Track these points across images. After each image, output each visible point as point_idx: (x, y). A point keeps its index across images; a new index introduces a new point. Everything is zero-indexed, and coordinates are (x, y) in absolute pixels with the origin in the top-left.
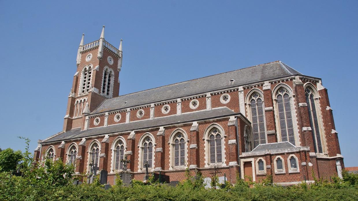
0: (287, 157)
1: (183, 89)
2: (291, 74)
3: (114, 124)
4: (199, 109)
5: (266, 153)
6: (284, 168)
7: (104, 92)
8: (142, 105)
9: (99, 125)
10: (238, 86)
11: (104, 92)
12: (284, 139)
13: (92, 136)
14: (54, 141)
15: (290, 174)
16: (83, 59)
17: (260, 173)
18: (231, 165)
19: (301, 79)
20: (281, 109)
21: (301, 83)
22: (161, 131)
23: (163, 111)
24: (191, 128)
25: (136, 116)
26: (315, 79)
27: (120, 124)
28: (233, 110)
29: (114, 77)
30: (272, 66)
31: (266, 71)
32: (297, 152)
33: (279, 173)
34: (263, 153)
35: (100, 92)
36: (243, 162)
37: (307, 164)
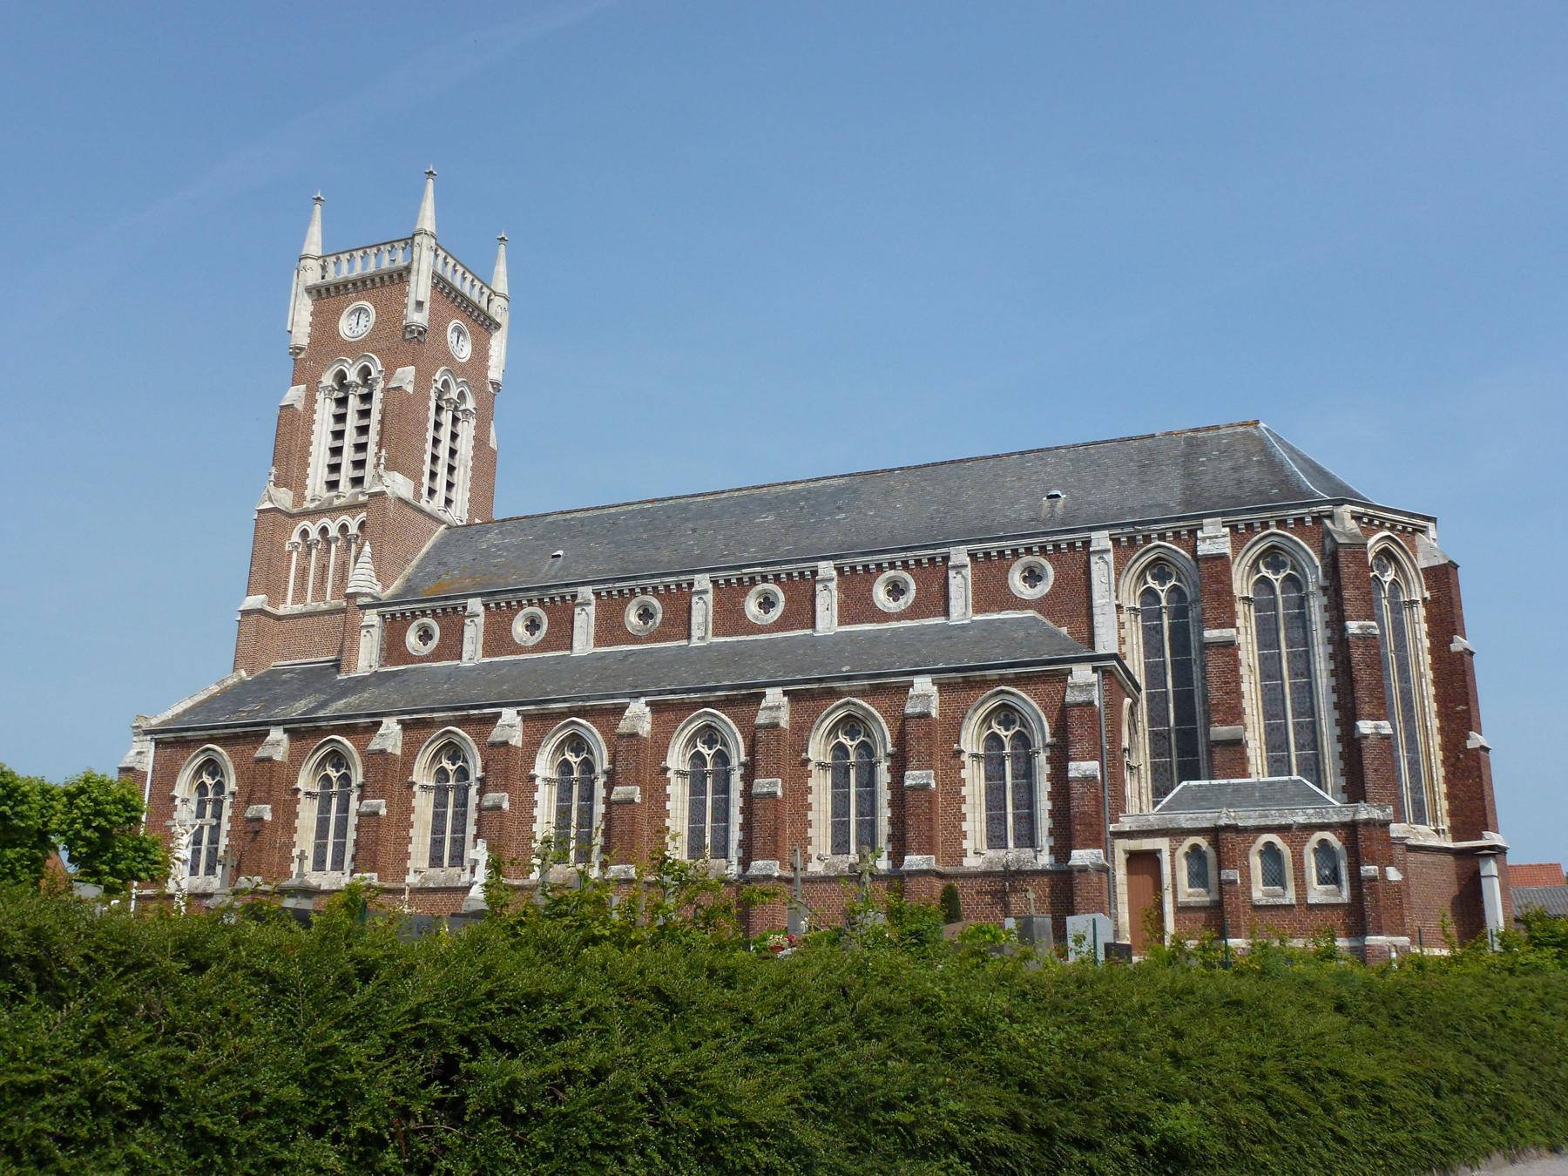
0: (1304, 842)
1: (829, 514)
2: (1312, 494)
3: (512, 653)
4: (913, 612)
5: (1222, 822)
6: (1291, 885)
7: (432, 492)
8: (653, 576)
9: (432, 653)
10: (1091, 529)
11: (432, 492)
12: (1278, 764)
13: (433, 710)
14: (227, 727)
15: (1312, 907)
16: (324, 324)
17: (1192, 899)
18: (1079, 863)
19: (1357, 518)
20: (1267, 636)
21: (1356, 535)
22: (770, 708)
23: (752, 607)
24: (908, 704)
25: (622, 626)
26: (1414, 521)
27: (547, 655)
28: (1064, 630)
29: (473, 422)
30: (1230, 445)
31: (1203, 464)
32: (1343, 825)
33: (1271, 901)
34: (1206, 819)
35: (418, 495)
36: (1126, 852)
37: (1383, 873)
